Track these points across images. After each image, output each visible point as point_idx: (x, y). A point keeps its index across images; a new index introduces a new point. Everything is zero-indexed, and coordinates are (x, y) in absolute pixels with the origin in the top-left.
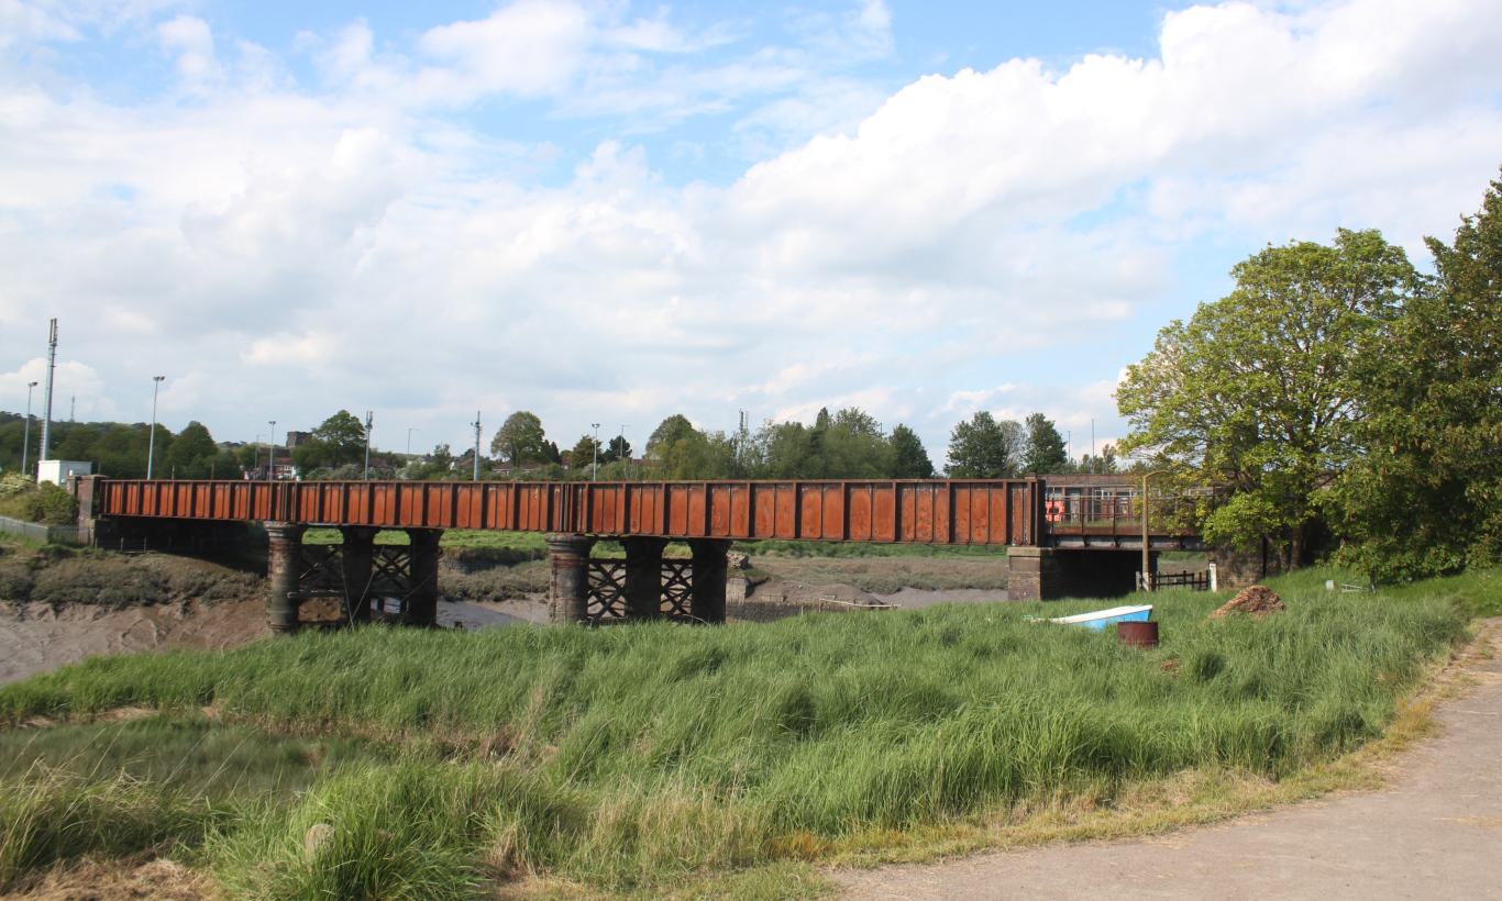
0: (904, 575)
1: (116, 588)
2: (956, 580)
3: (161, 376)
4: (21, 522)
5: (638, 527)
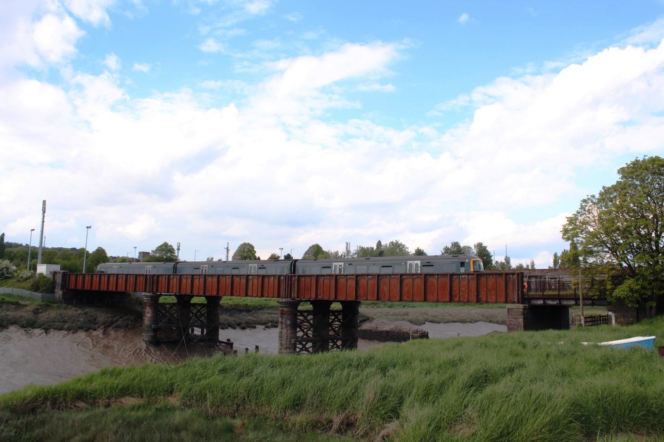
0: (425, 316)
1: (73, 322)
2: (449, 319)
3: (89, 226)
4: (30, 292)
5: (322, 295)
